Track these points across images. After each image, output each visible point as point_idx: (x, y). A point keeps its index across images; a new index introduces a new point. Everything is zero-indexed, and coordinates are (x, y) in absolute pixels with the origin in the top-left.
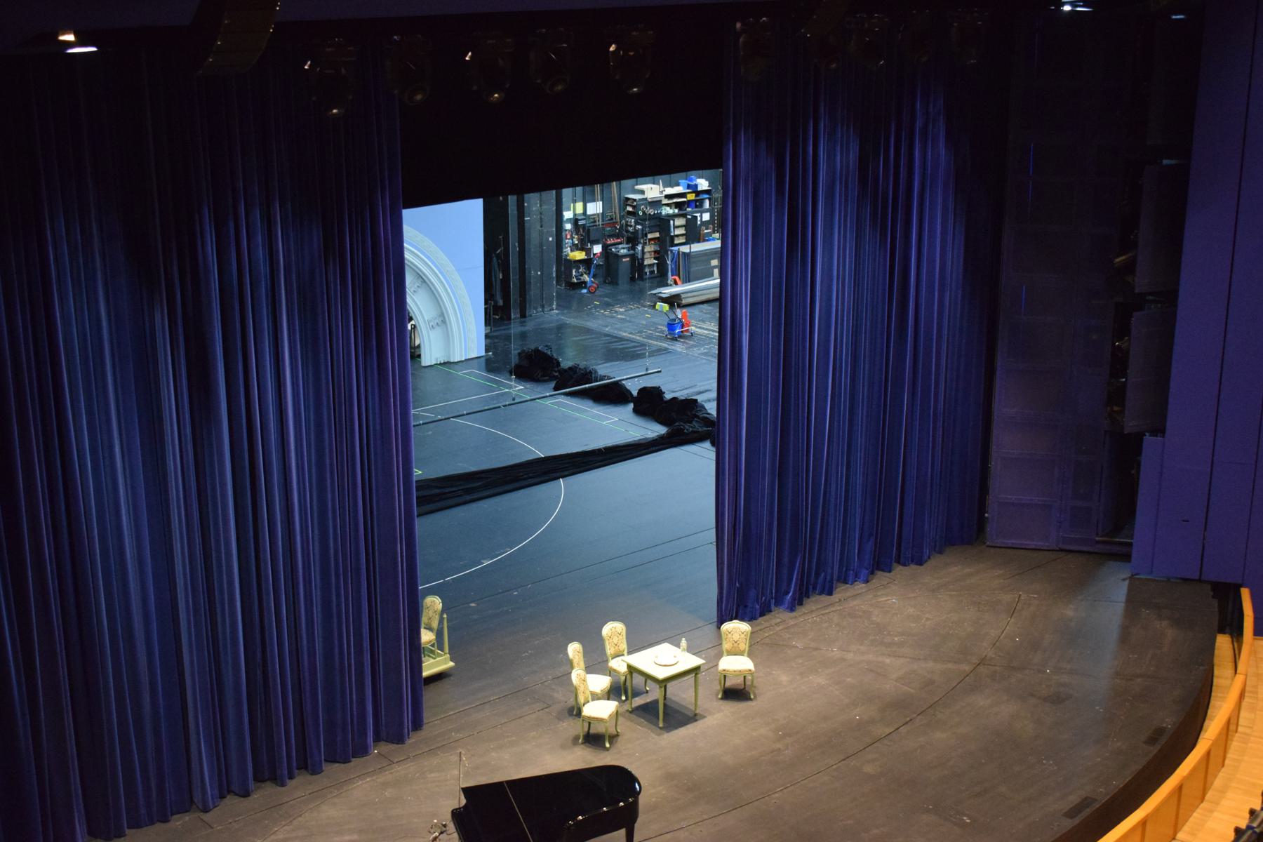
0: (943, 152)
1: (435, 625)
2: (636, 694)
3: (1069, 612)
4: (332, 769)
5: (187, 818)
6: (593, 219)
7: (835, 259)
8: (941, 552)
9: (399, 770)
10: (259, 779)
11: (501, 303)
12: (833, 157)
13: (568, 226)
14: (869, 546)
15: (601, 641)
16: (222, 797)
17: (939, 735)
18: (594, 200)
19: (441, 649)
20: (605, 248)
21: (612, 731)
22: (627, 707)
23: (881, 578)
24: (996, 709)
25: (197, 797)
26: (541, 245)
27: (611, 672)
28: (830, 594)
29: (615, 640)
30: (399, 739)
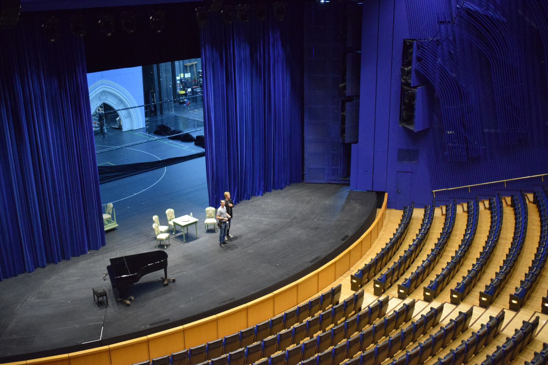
0: (281, 51)
1: (111, 212)
2: (177, 232)
3: (327, 202)
4: (73, 259)
5: (23, 275)
6: (187, 79)
7: (244, 88)
8: (289, 185)
9: (96, 258)
10: (48, 262)
11: (153, 109)
12: (241, 53)
13: (178, 82)
14: (262, 184)
15: (165, 215)
16: (35, 268)
17: (275, 241)
18: (187, 73)
19: (113, 220)
20: (192, 89)
21: (167, 243)
22: (174, 236)
23: (268, 194)
24: (296, 232)
25: (27, 268)
26: (167, 89)
27: (169, 225)
28: (249, 199)
29: (171, 215)
30: (97, 248)
